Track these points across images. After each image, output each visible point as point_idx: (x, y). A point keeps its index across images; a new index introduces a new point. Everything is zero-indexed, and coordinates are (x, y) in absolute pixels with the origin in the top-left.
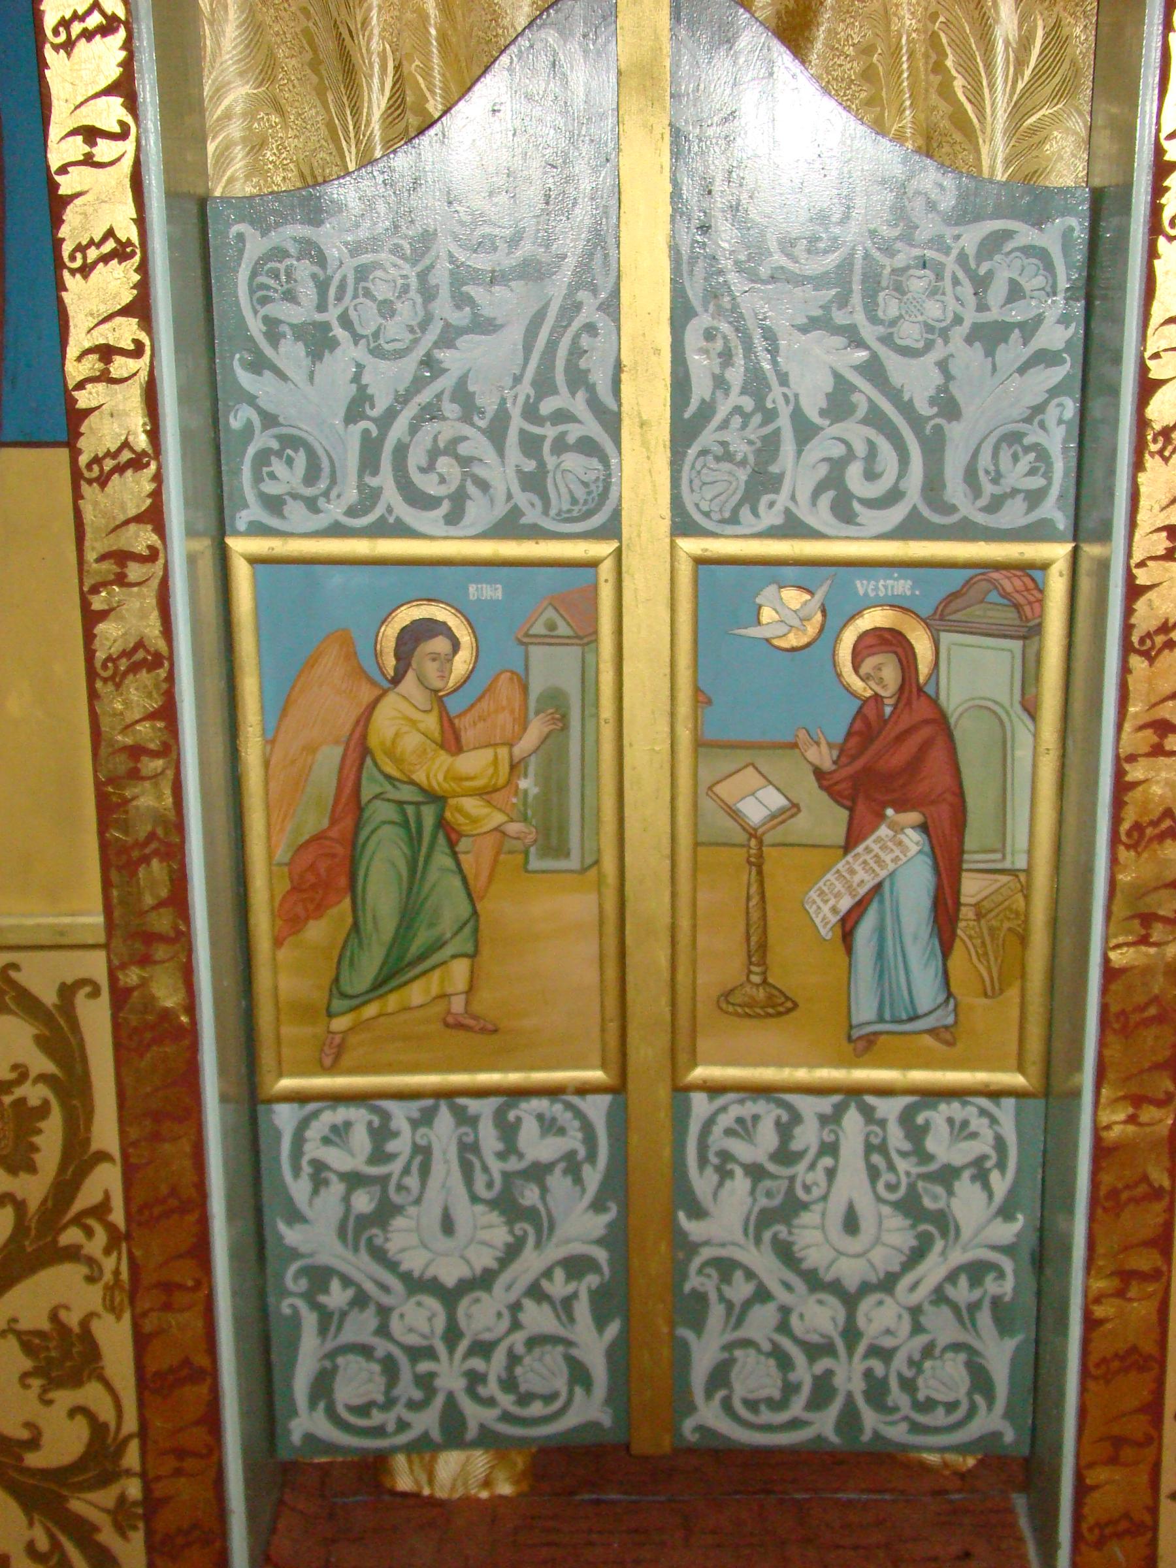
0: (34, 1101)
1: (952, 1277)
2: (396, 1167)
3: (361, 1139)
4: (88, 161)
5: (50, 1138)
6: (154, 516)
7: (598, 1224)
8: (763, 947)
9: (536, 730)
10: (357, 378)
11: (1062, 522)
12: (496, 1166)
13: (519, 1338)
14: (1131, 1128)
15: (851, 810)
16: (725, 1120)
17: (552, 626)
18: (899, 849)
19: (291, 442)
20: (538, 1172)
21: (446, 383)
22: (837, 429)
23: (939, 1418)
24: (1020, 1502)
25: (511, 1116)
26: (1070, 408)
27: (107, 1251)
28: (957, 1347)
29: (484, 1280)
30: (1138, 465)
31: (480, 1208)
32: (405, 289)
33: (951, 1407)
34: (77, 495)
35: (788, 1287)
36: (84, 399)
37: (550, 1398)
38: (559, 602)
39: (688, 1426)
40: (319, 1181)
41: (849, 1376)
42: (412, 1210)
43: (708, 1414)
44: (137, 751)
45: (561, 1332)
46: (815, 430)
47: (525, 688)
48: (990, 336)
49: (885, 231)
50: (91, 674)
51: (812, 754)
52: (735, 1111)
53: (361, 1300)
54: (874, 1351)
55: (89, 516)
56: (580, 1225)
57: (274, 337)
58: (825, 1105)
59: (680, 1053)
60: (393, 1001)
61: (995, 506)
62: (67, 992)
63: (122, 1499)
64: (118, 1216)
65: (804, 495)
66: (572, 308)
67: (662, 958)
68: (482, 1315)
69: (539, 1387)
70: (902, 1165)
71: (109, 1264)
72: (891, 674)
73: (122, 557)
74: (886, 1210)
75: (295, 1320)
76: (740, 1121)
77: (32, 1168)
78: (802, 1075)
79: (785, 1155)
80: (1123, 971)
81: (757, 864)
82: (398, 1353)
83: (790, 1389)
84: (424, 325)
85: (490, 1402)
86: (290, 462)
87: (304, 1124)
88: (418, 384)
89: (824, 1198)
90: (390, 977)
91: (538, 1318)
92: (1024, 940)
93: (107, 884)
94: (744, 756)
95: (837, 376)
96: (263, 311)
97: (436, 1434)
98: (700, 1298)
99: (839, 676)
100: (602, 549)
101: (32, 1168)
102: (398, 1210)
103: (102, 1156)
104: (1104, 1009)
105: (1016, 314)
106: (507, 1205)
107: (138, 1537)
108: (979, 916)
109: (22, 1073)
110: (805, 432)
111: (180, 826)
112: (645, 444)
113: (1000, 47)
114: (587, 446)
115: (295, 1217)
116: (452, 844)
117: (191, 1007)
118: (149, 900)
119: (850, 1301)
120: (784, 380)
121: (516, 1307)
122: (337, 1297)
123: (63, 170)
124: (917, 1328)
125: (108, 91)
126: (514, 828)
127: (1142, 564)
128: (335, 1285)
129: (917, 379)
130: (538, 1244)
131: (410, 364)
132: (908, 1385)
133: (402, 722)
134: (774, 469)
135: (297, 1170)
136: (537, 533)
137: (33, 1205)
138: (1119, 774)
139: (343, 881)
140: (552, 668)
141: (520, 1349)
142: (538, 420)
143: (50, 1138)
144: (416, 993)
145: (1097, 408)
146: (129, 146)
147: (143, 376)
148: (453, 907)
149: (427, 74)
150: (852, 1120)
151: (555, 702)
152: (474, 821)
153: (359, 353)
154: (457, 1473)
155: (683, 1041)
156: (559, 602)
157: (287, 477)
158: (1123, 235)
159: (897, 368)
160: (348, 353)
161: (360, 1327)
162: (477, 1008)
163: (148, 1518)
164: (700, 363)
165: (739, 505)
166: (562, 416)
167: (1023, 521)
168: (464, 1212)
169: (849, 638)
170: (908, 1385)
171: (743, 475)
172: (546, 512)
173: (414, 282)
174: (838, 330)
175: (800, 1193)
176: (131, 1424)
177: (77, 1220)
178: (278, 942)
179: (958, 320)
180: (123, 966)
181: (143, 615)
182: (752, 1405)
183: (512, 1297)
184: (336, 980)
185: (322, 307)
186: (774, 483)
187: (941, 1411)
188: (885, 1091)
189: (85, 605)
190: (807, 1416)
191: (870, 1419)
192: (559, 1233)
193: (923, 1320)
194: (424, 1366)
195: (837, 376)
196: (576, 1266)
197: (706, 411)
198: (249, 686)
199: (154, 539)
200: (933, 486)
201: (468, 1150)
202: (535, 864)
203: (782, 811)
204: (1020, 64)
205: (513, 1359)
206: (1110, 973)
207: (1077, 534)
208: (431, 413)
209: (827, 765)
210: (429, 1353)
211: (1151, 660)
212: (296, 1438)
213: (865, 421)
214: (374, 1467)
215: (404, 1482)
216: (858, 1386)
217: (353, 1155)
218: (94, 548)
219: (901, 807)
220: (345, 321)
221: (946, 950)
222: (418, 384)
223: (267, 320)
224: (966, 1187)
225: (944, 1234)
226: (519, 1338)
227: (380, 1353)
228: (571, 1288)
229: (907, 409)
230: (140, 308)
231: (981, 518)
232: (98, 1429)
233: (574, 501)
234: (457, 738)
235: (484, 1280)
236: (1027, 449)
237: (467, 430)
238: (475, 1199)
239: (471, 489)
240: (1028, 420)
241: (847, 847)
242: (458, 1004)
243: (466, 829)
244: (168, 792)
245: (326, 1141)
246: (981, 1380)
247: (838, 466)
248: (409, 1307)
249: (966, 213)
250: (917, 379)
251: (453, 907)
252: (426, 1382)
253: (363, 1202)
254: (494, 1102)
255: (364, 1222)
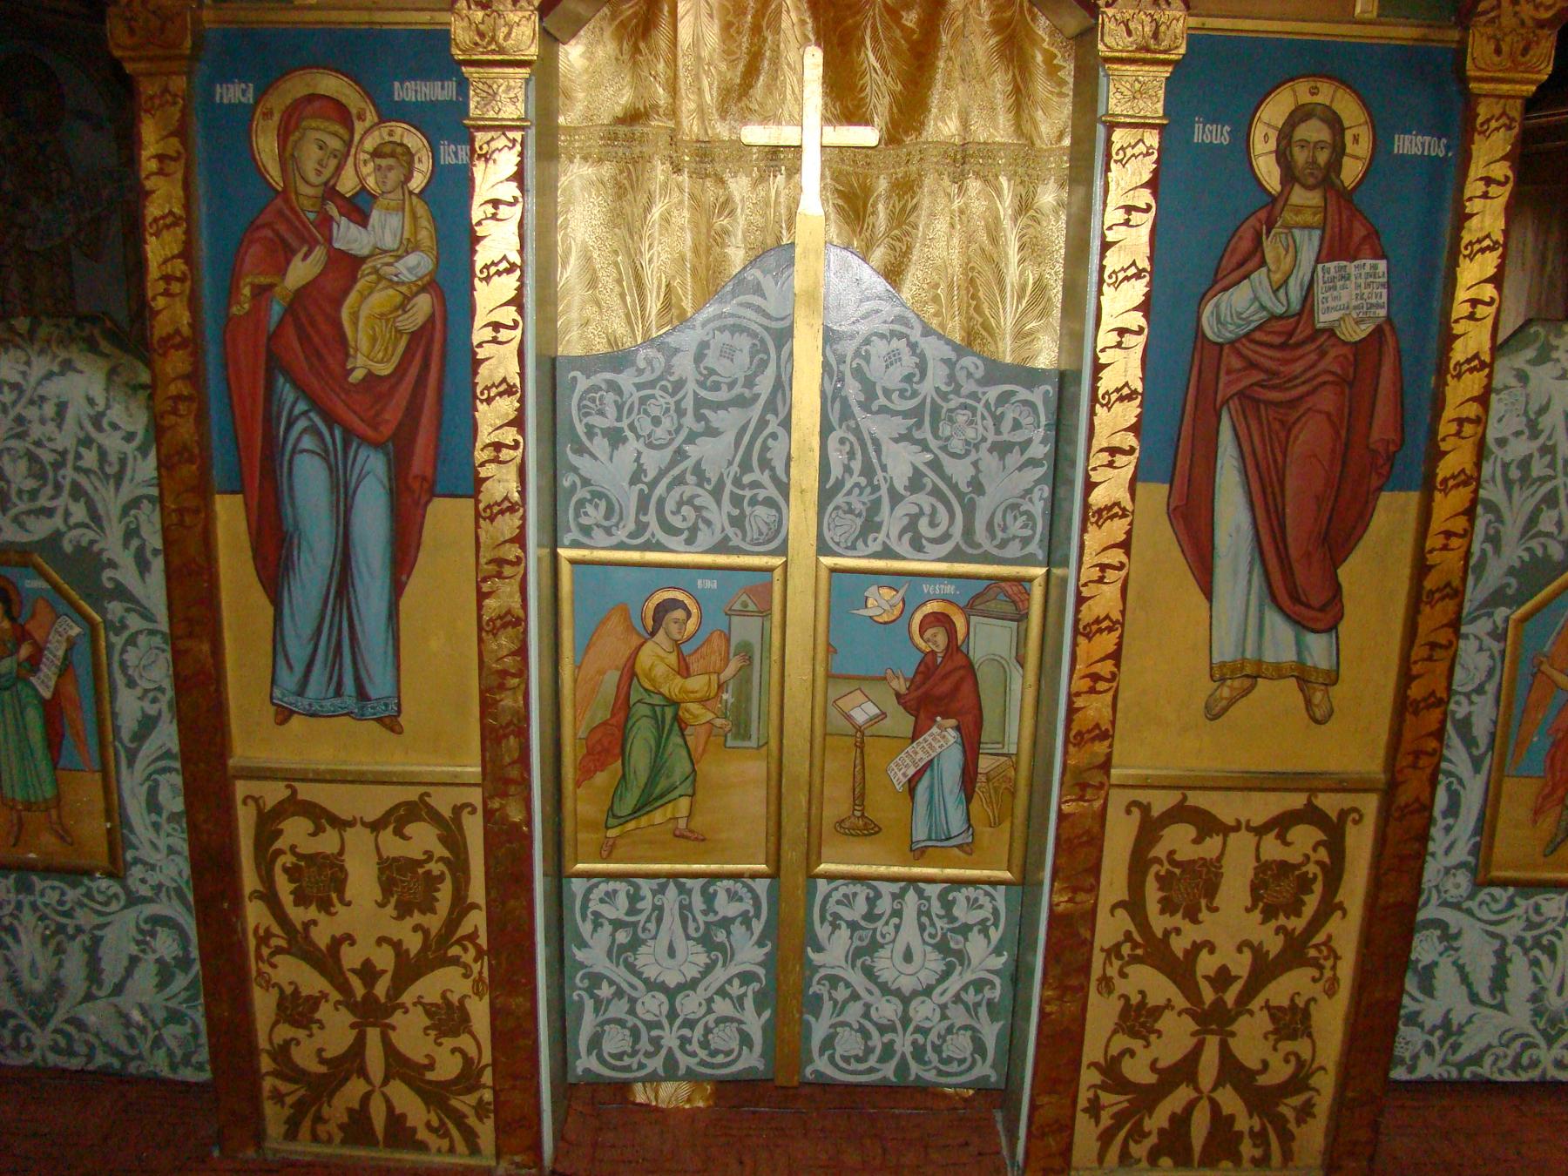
0: (436, 872)
1: (965, 988)
2: (642, 917)
3: (622, 901)
4: (495, 341)
5: (445, 894)
6: (520, 539)
7: (760, 954)
8: (863, 795)
9: (734, 665)
10: (637, 460)
11: (1041, 555)
12: (701, 919)
13: (711, 1018)
14: (1070, 905)
15: (917, 718)
16: (837, 896)
17: (745, 605)
18: (943, 740)
19: (600, 495)
20: (726, 923)
21: (688, 464)
22: (913, 498)
23: (954, 1067)
24: (999, 1116)
25: (711, 890)
26: (1047, 493)
27: (476, 961)
28: (965, 1028)
29: (692, 984)
30: (1084, 530)
31: (691, 943)
32: (668, 410)
33: (961, 1061)
34: (477, 526)
35: (870, 993)
36: (483, 473)
37: (728, 1054)
38: (750, 591)
39: (808, 1070)
40: (597, 925)
41: (903, 1043)
42: (651, 943)
43: (822, 1064)
44: (504, 673)
45: (737, 1015)
46: (903, 497)
47: (728, 640)
48: (1002, 449)
49: (944, 388)
50: (480, 629)
51: (895, 684)
52: (843, 890)
53: (619, 993)
54: (918, 1029)
55: (482, 539)
56: (749, 954)
57: (590, 433)
58: (895, 888)
59: (812, 854)
60: (644, 821)
61: (1003, 544)
62: (457, 810)
63: (481, 1100)
64: (483, 941)
65: (894, 533)
66: (763, 423)
67: (803, 799)
68: (690, 1005)
69: (721, 1046)
70: (939, 923)
71: (476, 967)
72: (942, 639)
73: (500, 562)
74: (929, 949)
75: (581, 1005)
76: (845, 895)
77: (433, 911)
78: (883, 870)
79: (871, 916)
80: (1070, 815)
81: (861, 747)
82: (640, 1024)
83: (869, 1051)
84: (678, 431)
85: (693, 1054)
86: (597, 506)
87: (589, 890)
88: (673, 464)
89: (893, 941)
90: (645, 805)
91: (723, 1007)
92: (1013, 794)
93: (483, 750)
94: (856, 684)
95: (916, 469)
96: (585, 420)
97: (661, 1072)
98: (818, 997)
99: (911, 638)
100: (777, 561)
101: (433, 911)
102: (644, 942)
103: (474, 906)
104: (1058, 838)
105: (1018, 437)
106: (706, 941)
107: (490, 1123)
108: (988, 780)
109: (429, 855)
110: (895, 498)
111: (527, 718)
112: (803, 502)
113: (1009, 288)
114: (769, 502)
115: (583, 944)
116: (682, 730)
117: (529, 821)
118: (507, 760)
119: (906, 1001)
120: (884, 468)
121: (710, 1000)
122: (605, 991)
123: (480, 345)
124: (944, 1017)
125: (507, 304)
126: (719, 722)
127: (1085, 585)
128: (605, 984)
129: (961, 472)
130: (724, 965)
131: (668, 453)
132: (937, 1049)
133: (655, 658)
134: (877, 519)
135: (584, 918)
136: (739, 551)
137: (434, 932)
138: (1070, 703)
139: (617, 750)
140: (745, 629)
141: (711, 1024)
142: (742, 487)
143: (445, 894)
144: (658, 817)
145: (1061, 492)
146: (518, 332)
147: (518, 460)
148: (681, 767)
149: (683, 285)
150: (911, 896)
151: (746, 652)
152: (696, 717)
153: (640, 446)
154: (670, 1094)
155: (814, 850)
156: (750, 591)
157: (594, 514)
158: (1077, 396)
159: (950, 466)
160: (633, 445)
161: (618, 1009)
162: (692, 825)
163: (496, 1112)
164: (837, 458)
165: (856, 539)
166: (755, 485)
167: (1019, 554)
168: (681, 945)
169: (918, 617)
170: (937, 1049)
171: (859, 522)
172: (744, 539)
173: (673, 407)
174: (915, 442)
175: (879, 937)
176: (487, 1057)
177: (458, 942)
178: (578, 784)
179: (984, 439)
180: (491, 797)
181: (511, 595)
182: (846, 1059)
183: (709, 994)
184: (611, 808)
185: (619, 419)
186: (877, 527)
187: (955, 1064)
188: (930, 880)
189: (479, 589)
190: (877, 1066)
191: (914, 1068)
192: (738, 958)
193: (948, 1013)
194: (654, 1033)
195: (916, 469)
196: (746, 978)
197: (839, 484)
198: (567, 634)
199: (519, 552)
200: (968, 531)
201: (685, 910)
202: (729, 744)
203: (877, 716)
204: (1019, 302)
205: (708, 1031)
206: (1062, 817)
207: (1049, 563)
208: (679, 480)
209: (903, 690)
210: (659, 1026)
211: (1090, 639)
212: (579, 1071)
213: (931, 494)
214: (624, 1087)
215: (640, 1098)
216: (908, 1049)
217: (618, 910)
218: (486, 555)
219: (945, 716)
220: (632, 427)
221: (969, 800)
222: (673, 464)
223: (587, 425)
224: (975, 936)
225: (962, 964)
226: (711, 1018)
227: (629, 1024)
228: (743, 990)
229: (954, 488)
230: (518, 422)
231: (995, 552)
232: (468, 1061)
233: (761, 533)
234: (688, 669)
235: (692, 984)
236: (1022, 514)
237: (700, 491)
238: (688, 937)
239: (701, 525)
240: (1023, 497)
241: (914, 739)
242: (682, 824)
243: (692, 721)
244: (520, 698)
245: (602, 901)
246: (979, 1047)
247: (914, 520)
248: (647, 999)
249: (988, 380)
250: (961, 472)
251: (681, 767)
252: (656, 1042)
253: (622, 937)
254: (701, 881)
255: (623, 948)
